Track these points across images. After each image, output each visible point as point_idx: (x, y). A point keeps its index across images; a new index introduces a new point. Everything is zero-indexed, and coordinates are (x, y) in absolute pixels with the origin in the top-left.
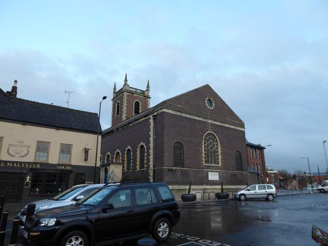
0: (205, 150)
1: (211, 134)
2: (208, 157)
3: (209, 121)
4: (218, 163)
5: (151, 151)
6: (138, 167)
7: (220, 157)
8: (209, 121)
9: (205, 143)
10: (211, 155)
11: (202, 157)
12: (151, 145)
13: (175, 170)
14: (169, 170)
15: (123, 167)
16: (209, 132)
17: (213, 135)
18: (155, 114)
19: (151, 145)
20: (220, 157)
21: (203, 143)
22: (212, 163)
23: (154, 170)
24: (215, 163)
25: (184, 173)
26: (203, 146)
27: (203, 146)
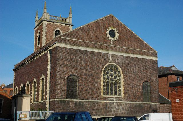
0: (104, 82)
1: (112, 65)
2: (108, 87)
3: (111, 53)
4: (120, 94)
5: (48, 84)
6: (40, 99)
7: (122, 88)
8: (111, 53)
9: (104, 75)
10: (112, 87)
11: (100, 89)
12: (48, 78)
13: (68, 102)
14: (61, 102)
15: (31, 99)
16: (110, 63)
17: (115, 67)
18: (51, 48)
19: (48, 78)
20: (122, 88)
21: (102, 74)
22: (112, 94)
23: (50, 102)
24: (116, 94)
25: (78, 104)
26: (102, 78)
27: (102, 78)
